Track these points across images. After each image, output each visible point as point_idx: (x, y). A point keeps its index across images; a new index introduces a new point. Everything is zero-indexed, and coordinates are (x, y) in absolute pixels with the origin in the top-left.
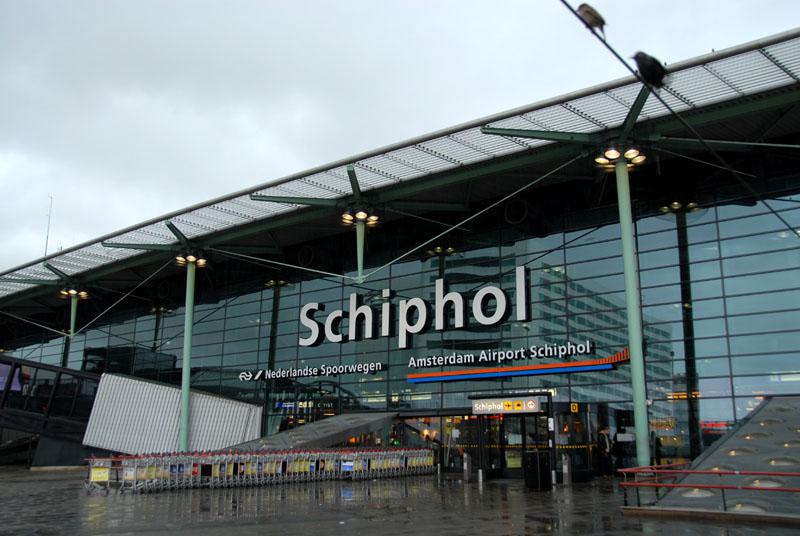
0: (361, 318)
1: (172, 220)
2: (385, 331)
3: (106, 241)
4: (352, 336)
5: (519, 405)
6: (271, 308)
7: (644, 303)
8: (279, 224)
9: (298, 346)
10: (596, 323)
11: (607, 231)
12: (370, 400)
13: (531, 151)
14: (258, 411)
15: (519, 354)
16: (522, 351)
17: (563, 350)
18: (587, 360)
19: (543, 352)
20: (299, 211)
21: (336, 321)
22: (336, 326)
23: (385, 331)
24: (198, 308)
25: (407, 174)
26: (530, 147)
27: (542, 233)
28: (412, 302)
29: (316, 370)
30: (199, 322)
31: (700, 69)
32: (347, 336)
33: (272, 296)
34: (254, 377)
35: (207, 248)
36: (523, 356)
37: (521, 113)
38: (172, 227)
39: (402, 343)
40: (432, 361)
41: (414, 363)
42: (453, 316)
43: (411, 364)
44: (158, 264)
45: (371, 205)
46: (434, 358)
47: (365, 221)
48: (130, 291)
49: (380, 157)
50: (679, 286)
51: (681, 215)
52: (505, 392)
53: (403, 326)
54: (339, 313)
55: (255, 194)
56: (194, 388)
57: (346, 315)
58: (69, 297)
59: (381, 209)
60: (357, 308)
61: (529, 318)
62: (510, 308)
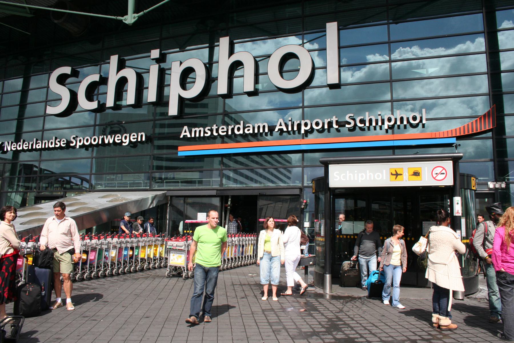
0: (122, 82)
2: (151, 95)
4: (110, 102)
5: (416, 174)
7: (341, 45)
12: (43, 193)
15: (330, 124)
22: (91, 92)
23: (151, 95)
27: (464, 312)
32: (104, 104)
39: (173, 110)
40: (211, 130)
43: (183, 134)
46: (215, 127)
51: (485, 53)
54: (96, 78)
57: (104, 81)
62: (210, 80)
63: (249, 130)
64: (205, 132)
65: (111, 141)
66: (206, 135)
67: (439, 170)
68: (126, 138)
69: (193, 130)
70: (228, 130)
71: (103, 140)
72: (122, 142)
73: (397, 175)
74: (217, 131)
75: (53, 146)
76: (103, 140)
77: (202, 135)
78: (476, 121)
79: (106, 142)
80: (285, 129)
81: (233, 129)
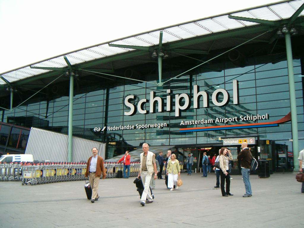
0: (156, 103)
1: (67, 56)
3: (32, 66)
4: (151, 111)
5: (245, 141)
6: (46, 107)
8: (117, 58)
9: (123, 115)
10: (219, 110)
11: (281, 64)
13: (129, 52)
14: (104, 145)
15: (235, 119)
16: (236, 118)
17: (255, 118)
18: (234, 125)
19: (246, 118)
20: (50, 72)
21: (143, 104)
24: (77, 96)
25: (88, 59)
26: (282, 18)
28: (181, 96)
29: (133, 127)
30: (66, 106)
31: (266, 8)
33: (47, 102)
34: (101, 130)
35: (80, 69)
36: (236, 120)
37: (121, 39)
38: (66, 59)
39: (177, 114)
41: (218, 121)
42: (174, 105)
43: (181, 124)
44: (54, 77)
45: (165, 50)
47: (162, 57)
48: (48, 86)
49: (177, 27)
50: (302, 91)
52: (227, 136)
53: (177, 107)
54: (145, 100)
55: (110, 44)
56: (74, 135)
57: (148, 101)
58: (284, 34)
59: (170, 52)
60: (154, 98)
61: (198, 107)
63: (206, 122)
64: (190, 123)
65: (153, 127)
66: (190, 124)
67: (252, 142)
68: (159, 125)
69: (208, 120)
70: (164, 124)
71: (150, 126)
72: (157, 127)
73: (240, 141)
74: (194, 122)
75: (129, 128)
76: (150, 126)
77: (188, 124)
78: (286, 117)
79: (151, 127)
80: (219, 122)
81: (200, 122)
